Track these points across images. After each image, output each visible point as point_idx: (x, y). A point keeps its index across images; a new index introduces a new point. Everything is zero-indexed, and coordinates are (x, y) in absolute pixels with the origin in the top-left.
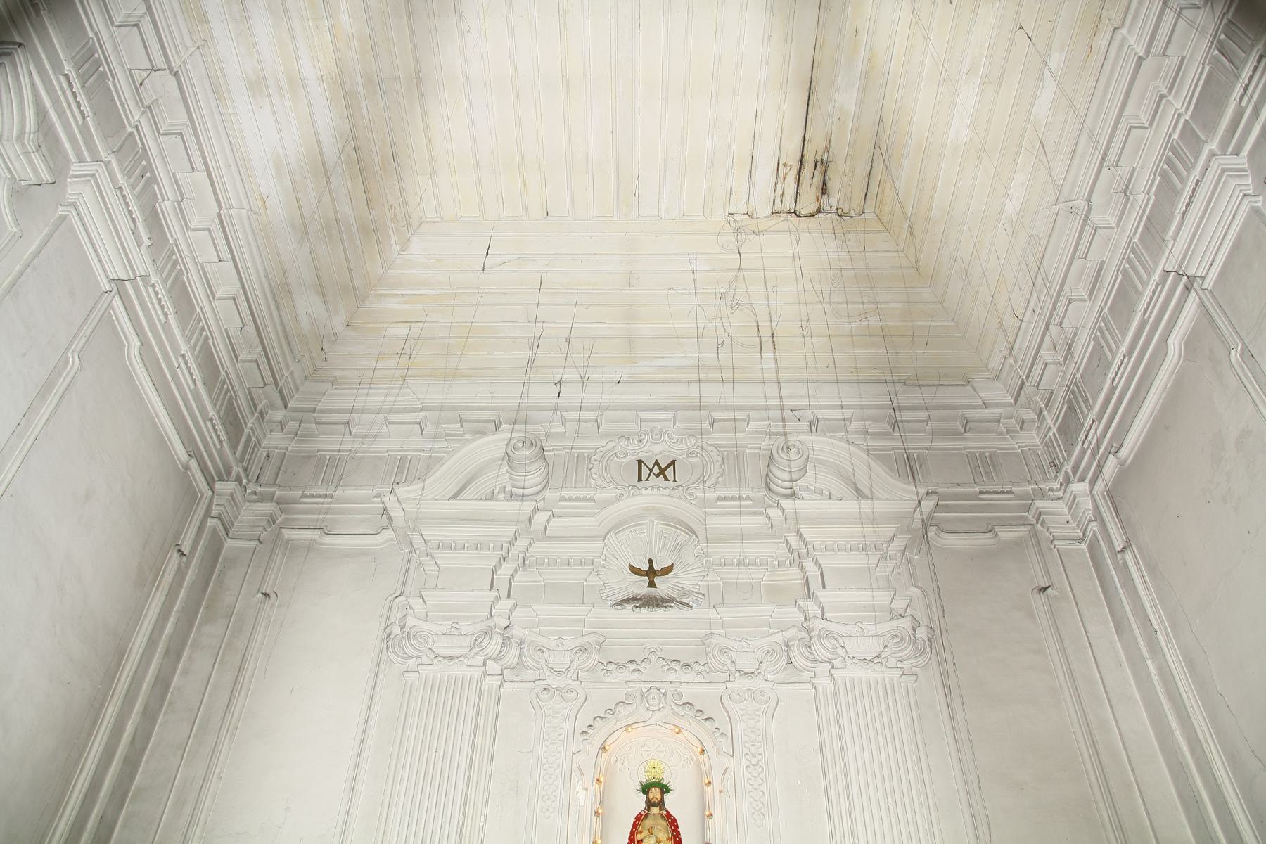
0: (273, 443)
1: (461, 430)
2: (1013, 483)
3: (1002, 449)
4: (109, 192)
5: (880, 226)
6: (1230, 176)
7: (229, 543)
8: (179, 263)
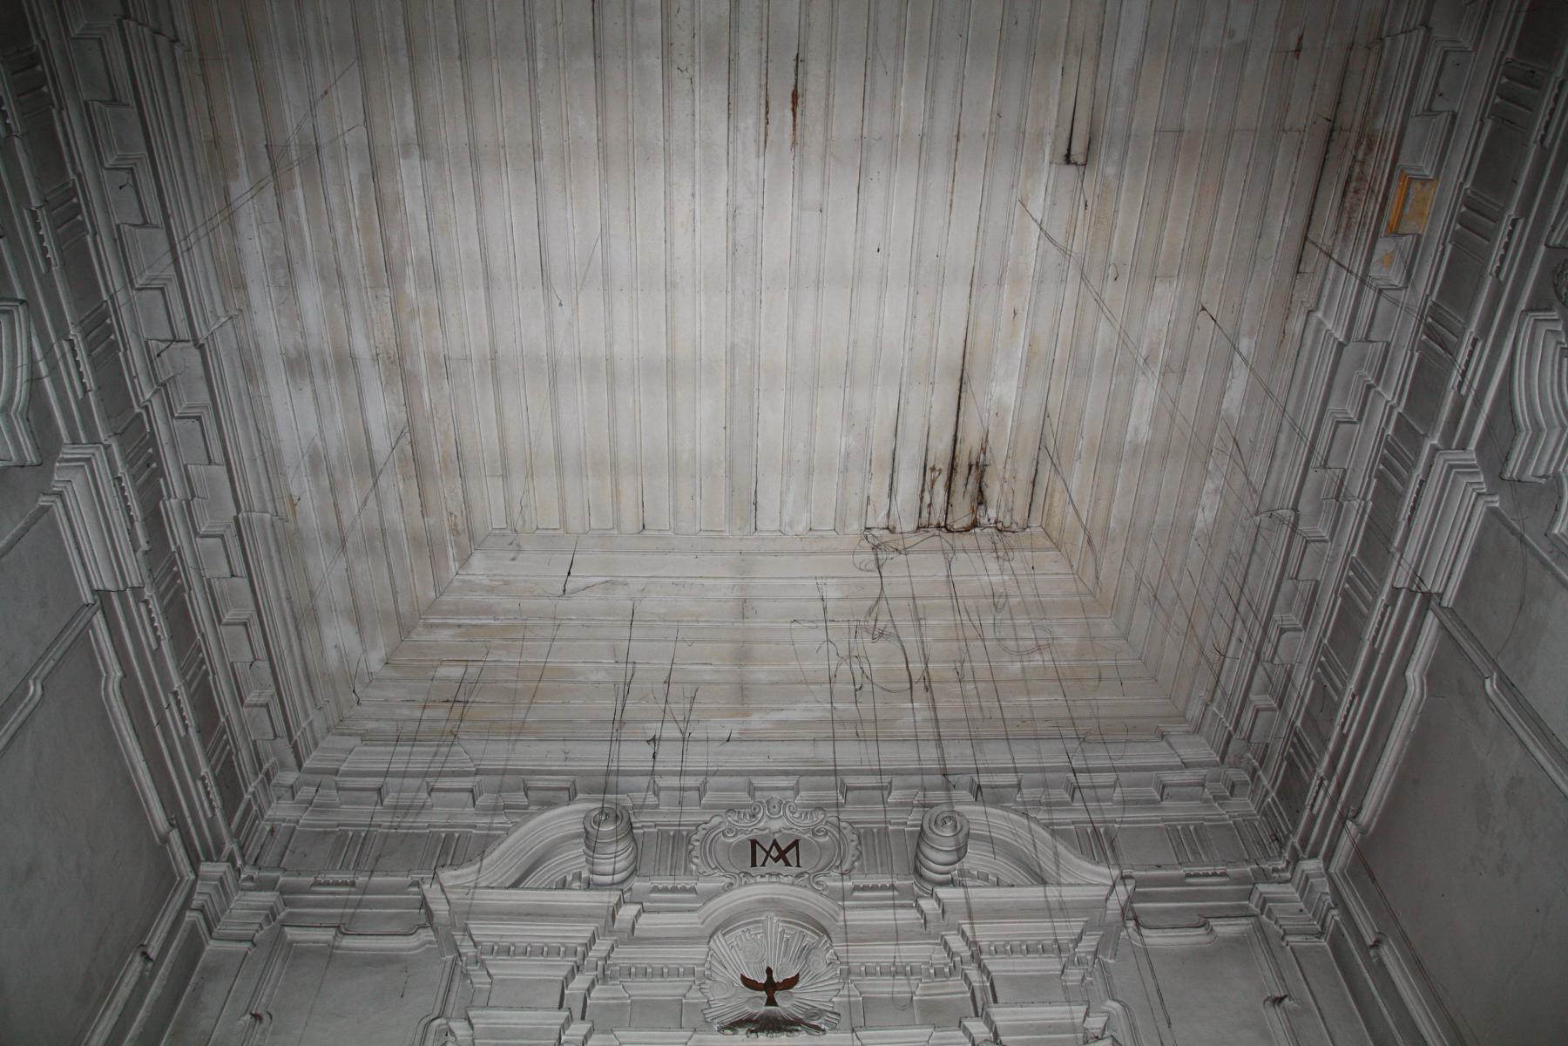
0: (280, 814)
1: (525, 801)
2: (1227, 864)
3: (1209, 820)
4: (105, 482)
5: (1048, 543)
6: (1459, 473)
7: (212, 946)
8: (180, 577)
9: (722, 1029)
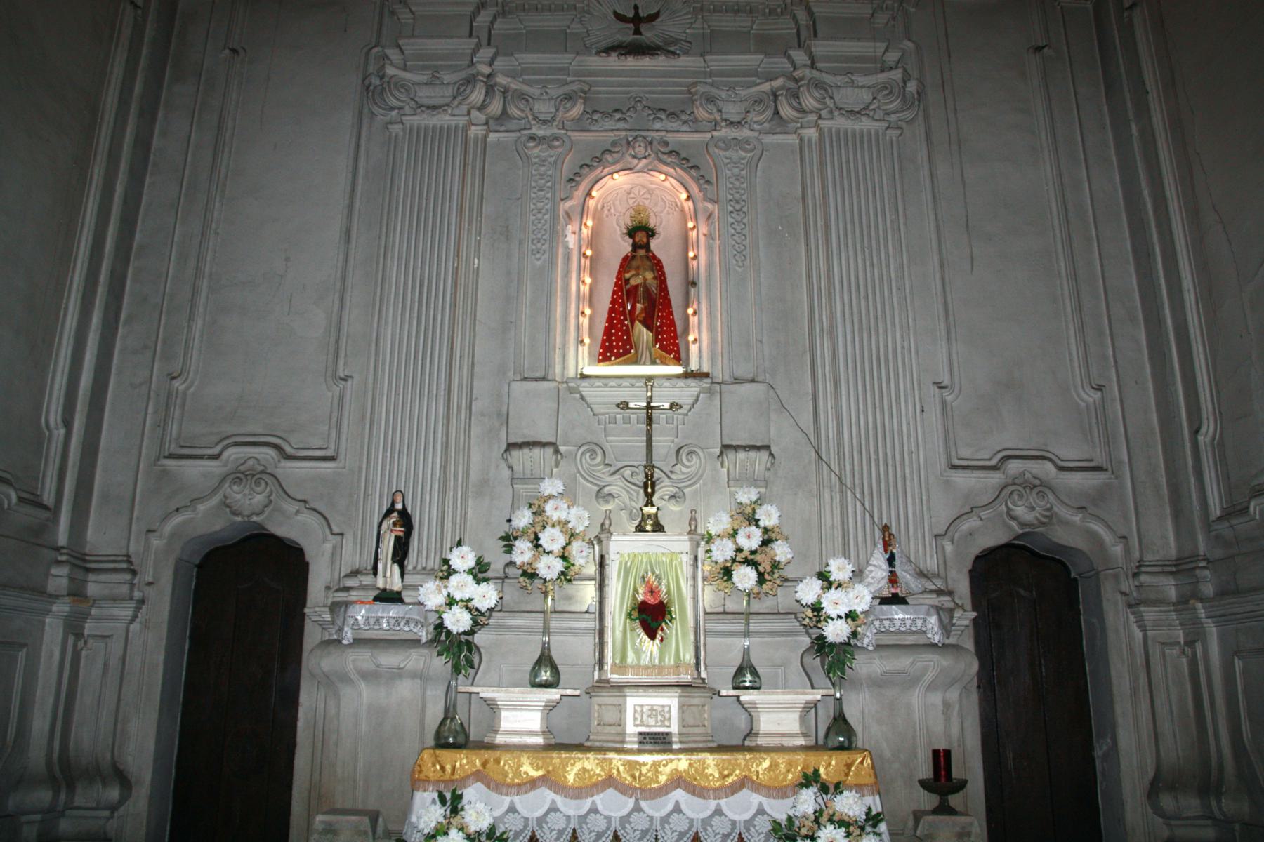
9: (598, 53)
